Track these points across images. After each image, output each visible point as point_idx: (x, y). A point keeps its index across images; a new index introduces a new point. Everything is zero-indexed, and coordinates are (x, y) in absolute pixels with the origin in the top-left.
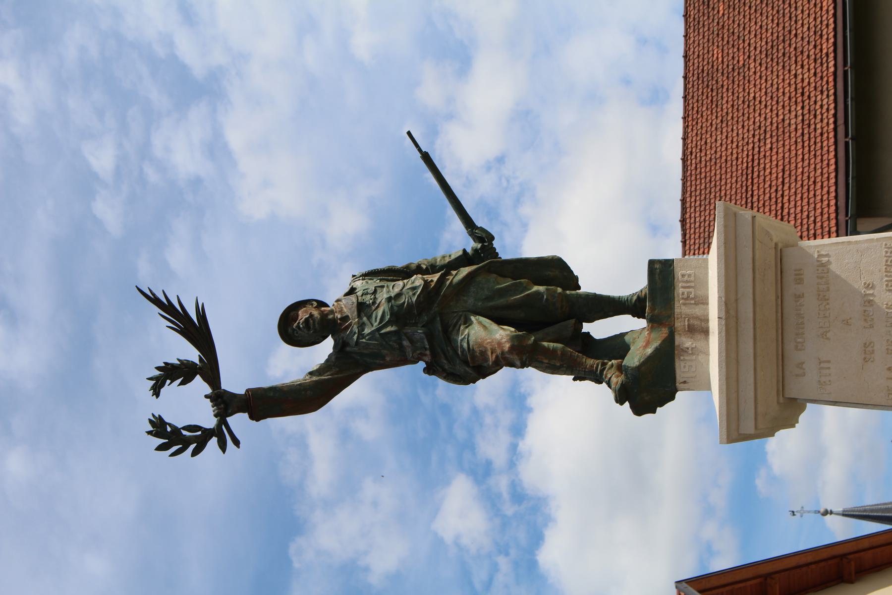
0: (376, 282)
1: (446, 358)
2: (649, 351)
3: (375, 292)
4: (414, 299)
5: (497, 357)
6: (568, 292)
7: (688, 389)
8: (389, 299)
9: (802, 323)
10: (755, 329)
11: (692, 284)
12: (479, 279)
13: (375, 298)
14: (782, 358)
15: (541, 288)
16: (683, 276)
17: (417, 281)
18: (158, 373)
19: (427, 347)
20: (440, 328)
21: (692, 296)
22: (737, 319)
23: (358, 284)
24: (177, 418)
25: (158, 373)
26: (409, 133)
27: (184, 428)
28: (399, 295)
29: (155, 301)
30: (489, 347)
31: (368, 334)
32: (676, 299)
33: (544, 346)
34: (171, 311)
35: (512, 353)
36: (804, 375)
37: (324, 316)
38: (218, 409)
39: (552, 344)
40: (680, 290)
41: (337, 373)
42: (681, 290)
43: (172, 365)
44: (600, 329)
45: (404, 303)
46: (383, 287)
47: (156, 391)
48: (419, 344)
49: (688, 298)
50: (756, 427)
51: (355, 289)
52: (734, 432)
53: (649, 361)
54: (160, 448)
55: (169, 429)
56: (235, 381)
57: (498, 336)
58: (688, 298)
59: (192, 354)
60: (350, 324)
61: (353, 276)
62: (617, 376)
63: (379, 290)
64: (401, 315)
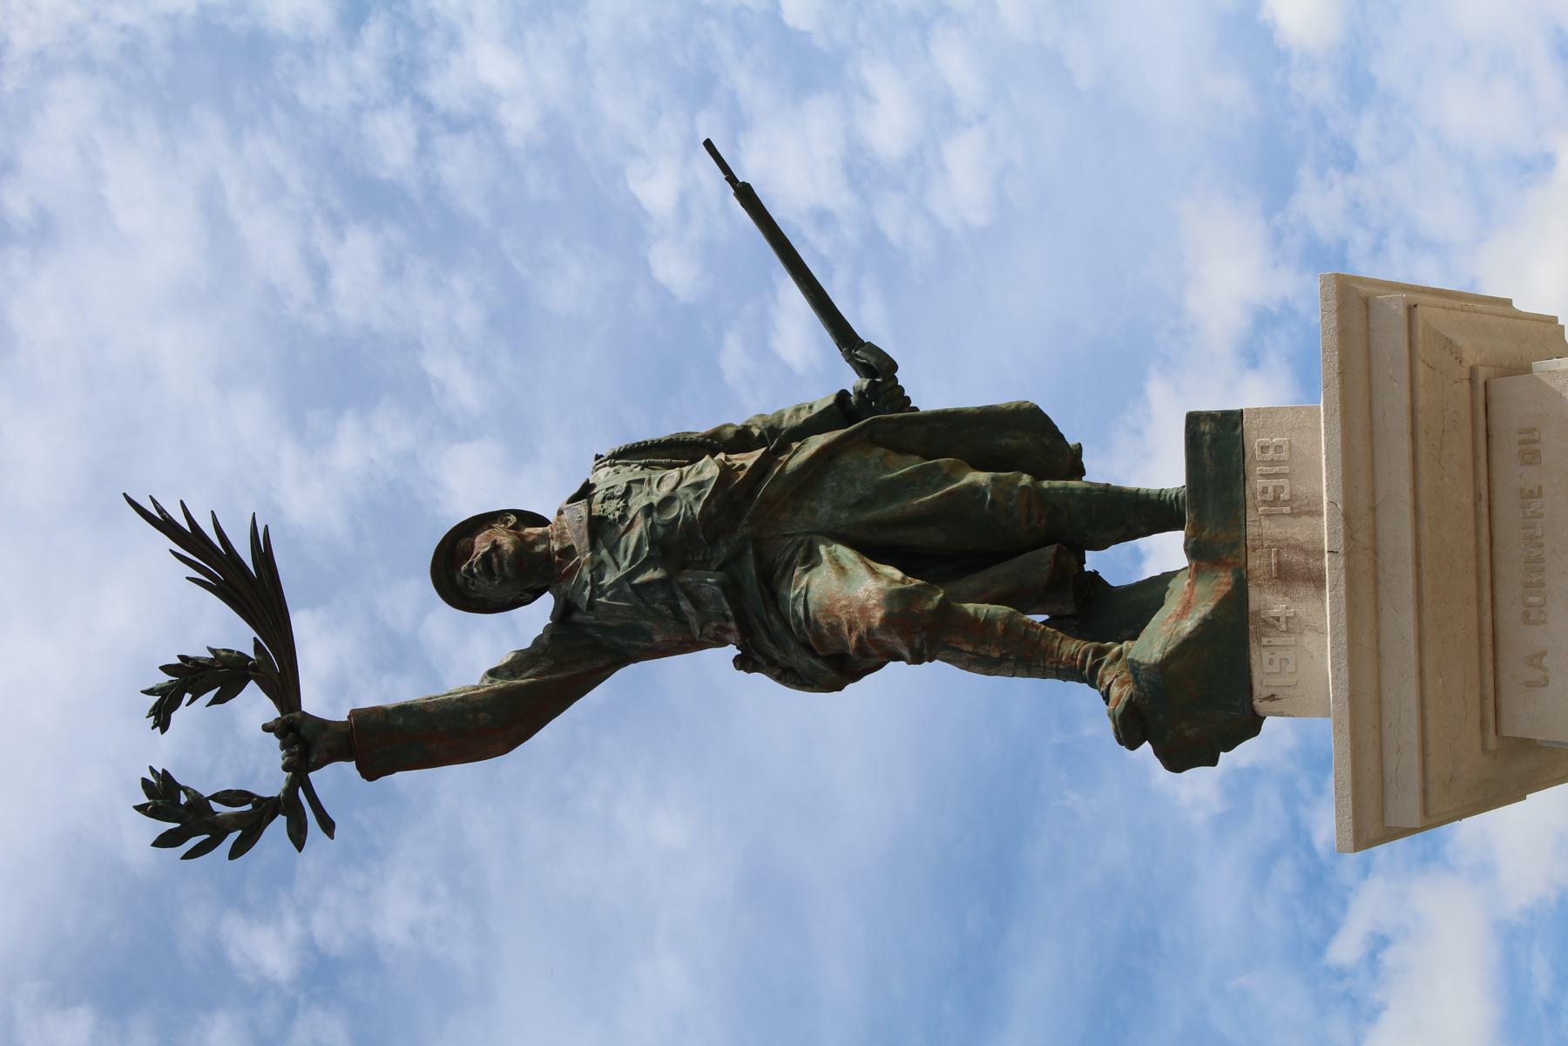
0: (631, 472)
1: (773, 641)
2: (1188, 625)
3: (627, 492)
4: (698, 509)
5: (860, 639)
6: (1045, 484)
7: (1281, 714)
8: (649, 510)
9: (1540, 559)
10: (1418, 577)
11: (1285, 469)
12: (846, 460)
13: (626, 507)
14: (1492, 642)
15: (982, 477)
16: (1264, 449)
17: (709, 469)
18: (165, 679)
19: (730, 613)
20: (753, 573)
21: (1284, 496)
22: (1375, 552)
23: (604, 479)
24: (205, 775)
25: (165, 679)
26: (708, 144)
27: (215, 797)
28: (668, 501)
29: (164, 524)
30: (844, 617)
31: (611, 586)
32: (1249, 503)
33: (966, 614)
34: (196, 545)
35: (888, 632)
36: (1545, 682)
37: (523, 546)
38: (289, 754)
39: (985, 609)
40: (1258, 483)
41: (550, 670)
42: (1260, 483)
43: (195, 661)
44: (1116, 564)
45: (678, 517)
46: (641, 481)
47: (162, 717)
48: (711, 609)
49: (1276, 501)
50: (1425, 811)
51: (593, 486)
52: (1372, 825)
53: (1186, 649)
54: (163, 841)
55: (184, 799)
56: (322, 698)
57: (861, 593)
58: (1276, 501)
59: (239, 636)
60: (577, 564)
61: (598, 457)
62: (1123, 683)
63: (635, 488)
64: (673, 544)
